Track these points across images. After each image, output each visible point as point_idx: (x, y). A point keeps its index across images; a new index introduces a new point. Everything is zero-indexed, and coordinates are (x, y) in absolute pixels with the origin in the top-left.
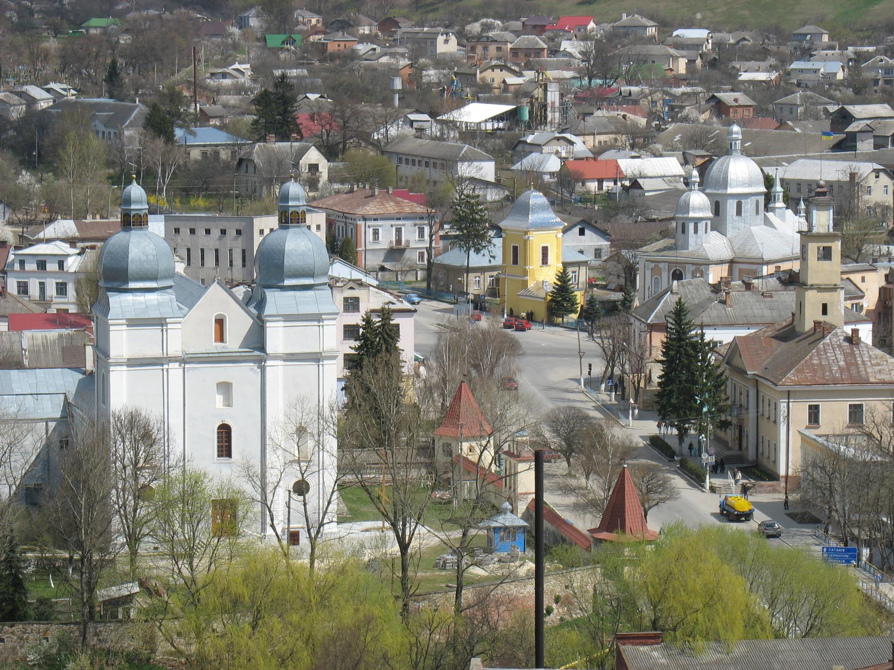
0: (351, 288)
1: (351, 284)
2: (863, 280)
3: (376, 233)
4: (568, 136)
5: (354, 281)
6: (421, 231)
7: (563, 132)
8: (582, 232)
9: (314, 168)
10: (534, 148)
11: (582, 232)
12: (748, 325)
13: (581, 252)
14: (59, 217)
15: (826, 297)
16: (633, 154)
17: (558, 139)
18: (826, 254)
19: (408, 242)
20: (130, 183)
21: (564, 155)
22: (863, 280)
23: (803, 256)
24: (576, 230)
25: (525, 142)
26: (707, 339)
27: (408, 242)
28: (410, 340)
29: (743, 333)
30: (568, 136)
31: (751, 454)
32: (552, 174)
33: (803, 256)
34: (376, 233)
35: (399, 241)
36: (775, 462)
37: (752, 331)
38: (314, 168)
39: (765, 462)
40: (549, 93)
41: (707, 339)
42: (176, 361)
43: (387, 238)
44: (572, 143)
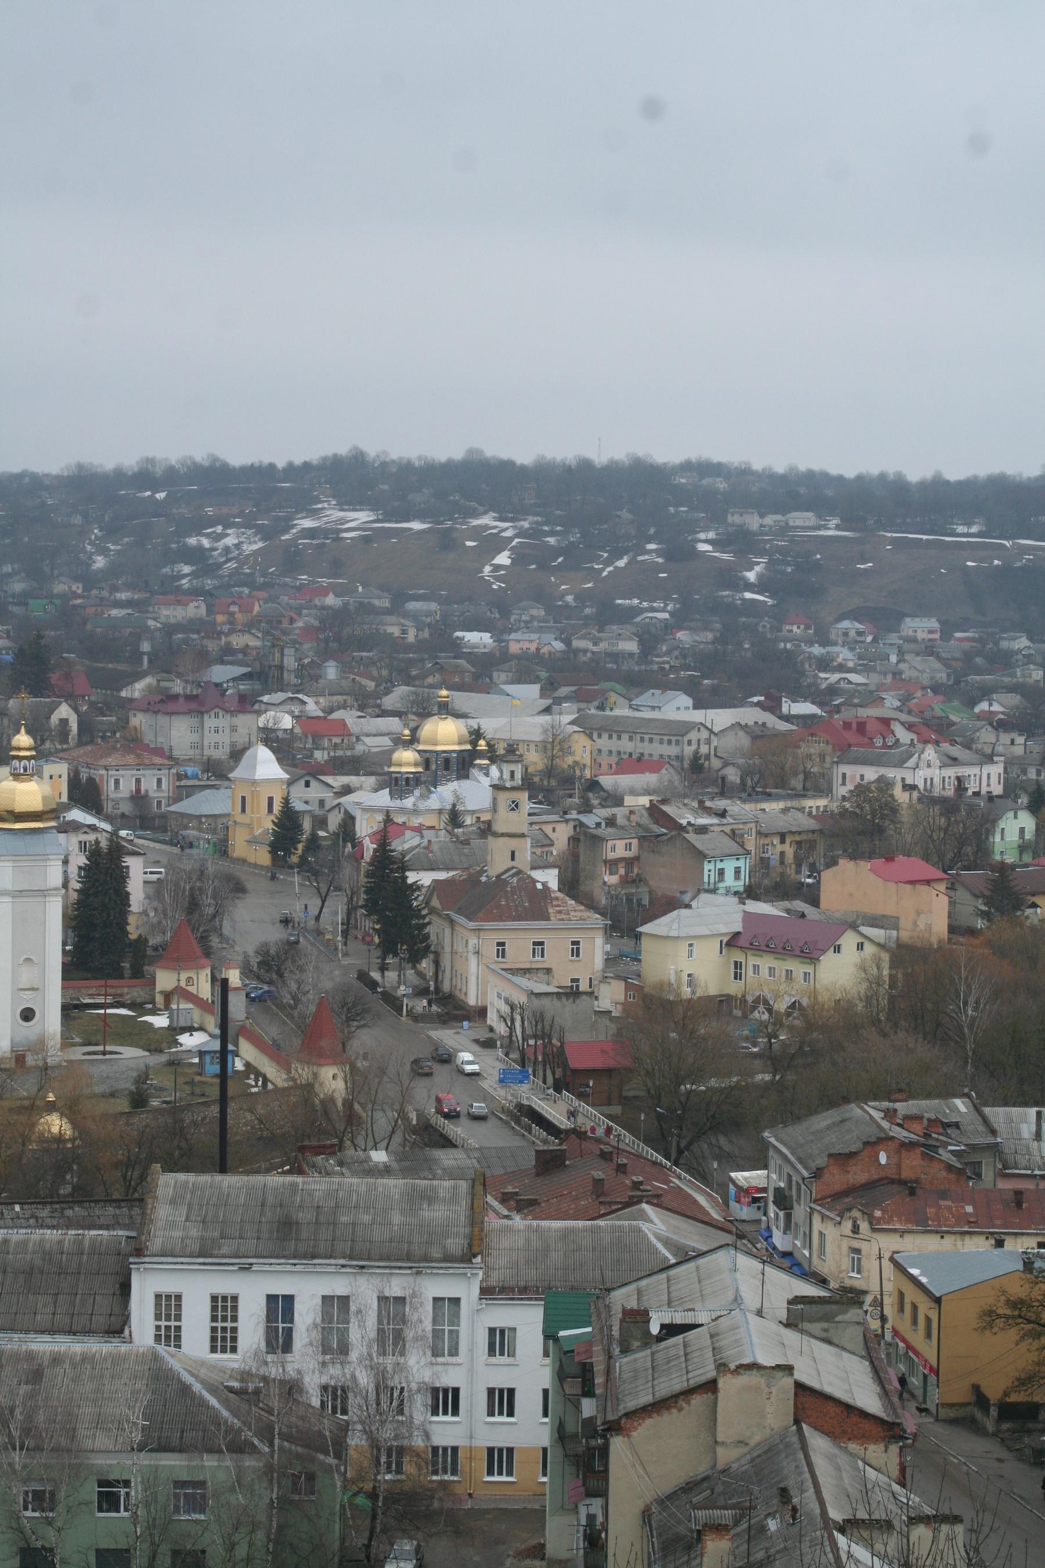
0: (85, 832)
1: (86, 829)
2: (554, 830)
3: (117, 782)
4: (300, 696)
5: (89, 826)
6: (159, 781)
7: (298, 692)
8: (307, 784)
9: (64, 722)
10: (270, 707)
11: (307, 784)
12: (447, 869)
13: (306, 802)
14: (860, 1007)
15: (513, 843)
16: (360, 714)
17: (292, 699)
18: (515, 806)
19: (147, 791)
20: (18, 732)
21: (297, 713)
22: (554, 830)
23: (494, 809)
24: (302, 782)
25: (261, 701)
26: (410, 881)
27: (147, 791)
28: (138, 876)
29: (442, 875)
30: (300, 696)
31: (446, 987)
32: (285, 730)
33: (494, 809)
34: (117, 782)
35: (138, 790)
36: (466, 994)
37: (451, 874)
38: (64, 722)
39: (458, 993)
40: (285, 658)
41: (410, 881)
42: (821, 1510)
43: (127, 786)
44: (304, 703)
